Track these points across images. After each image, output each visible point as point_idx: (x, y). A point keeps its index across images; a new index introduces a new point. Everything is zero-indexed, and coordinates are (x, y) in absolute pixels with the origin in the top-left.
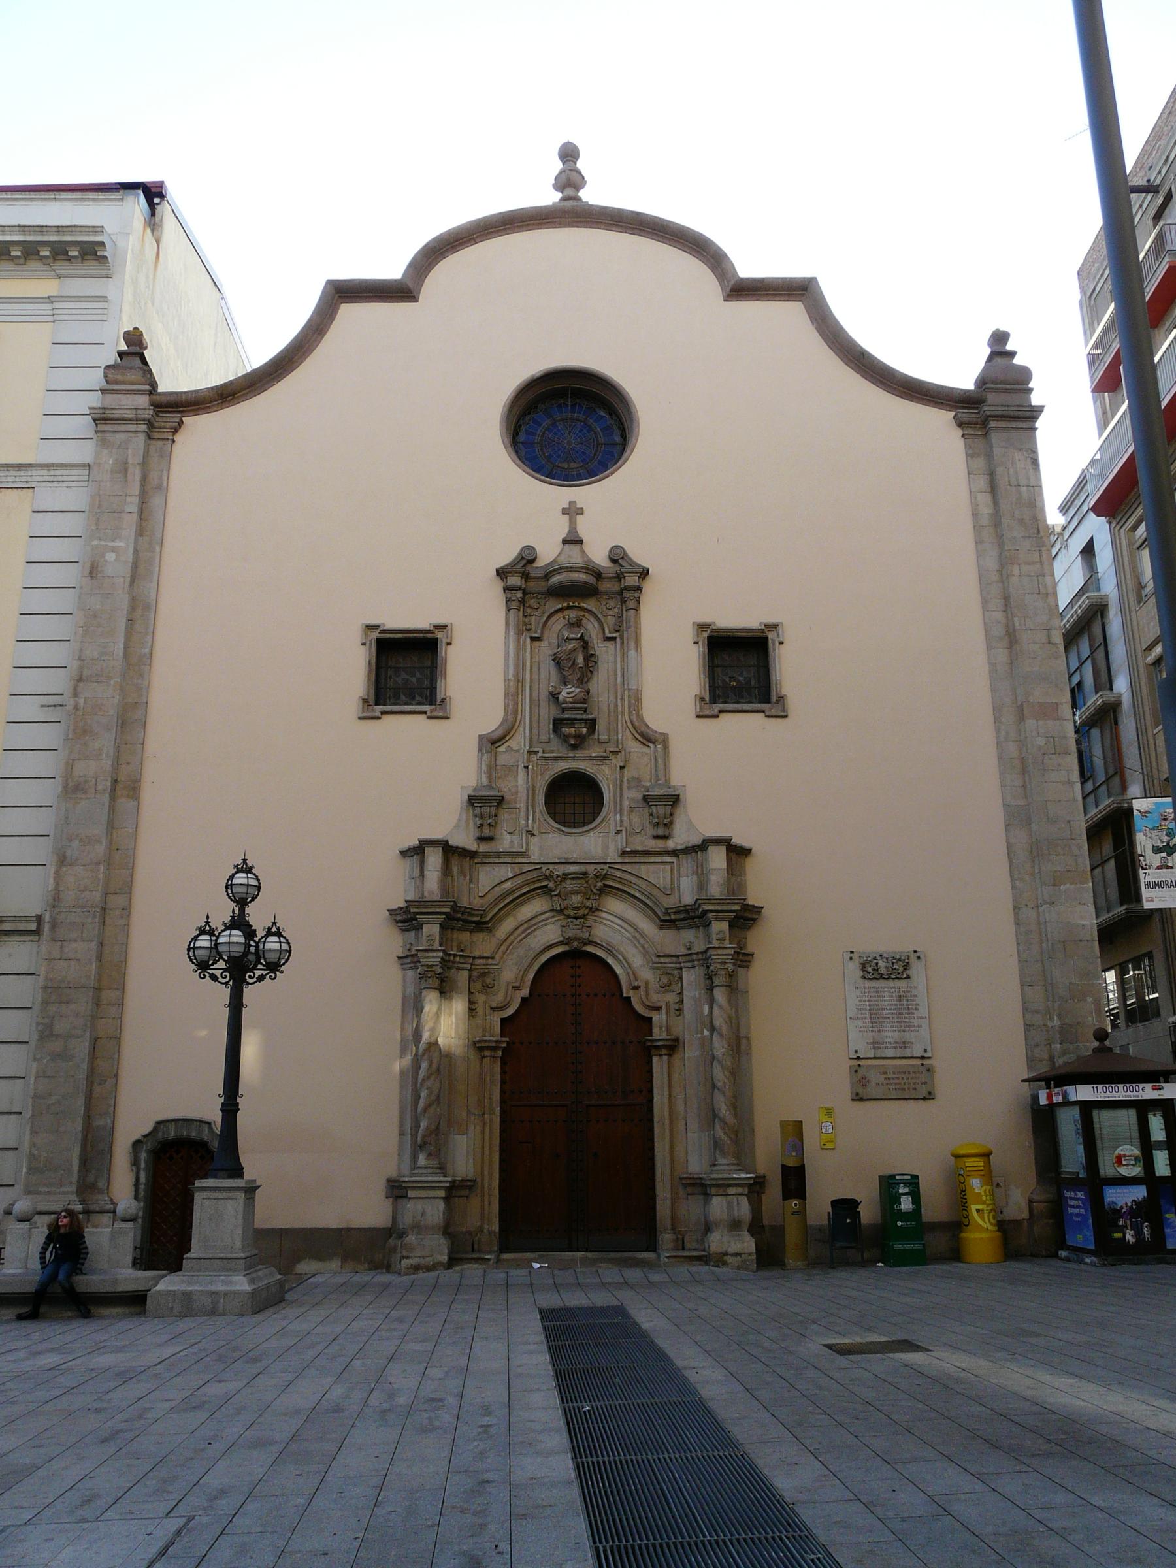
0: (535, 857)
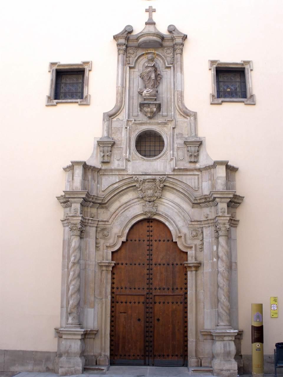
0: (130, 172)
